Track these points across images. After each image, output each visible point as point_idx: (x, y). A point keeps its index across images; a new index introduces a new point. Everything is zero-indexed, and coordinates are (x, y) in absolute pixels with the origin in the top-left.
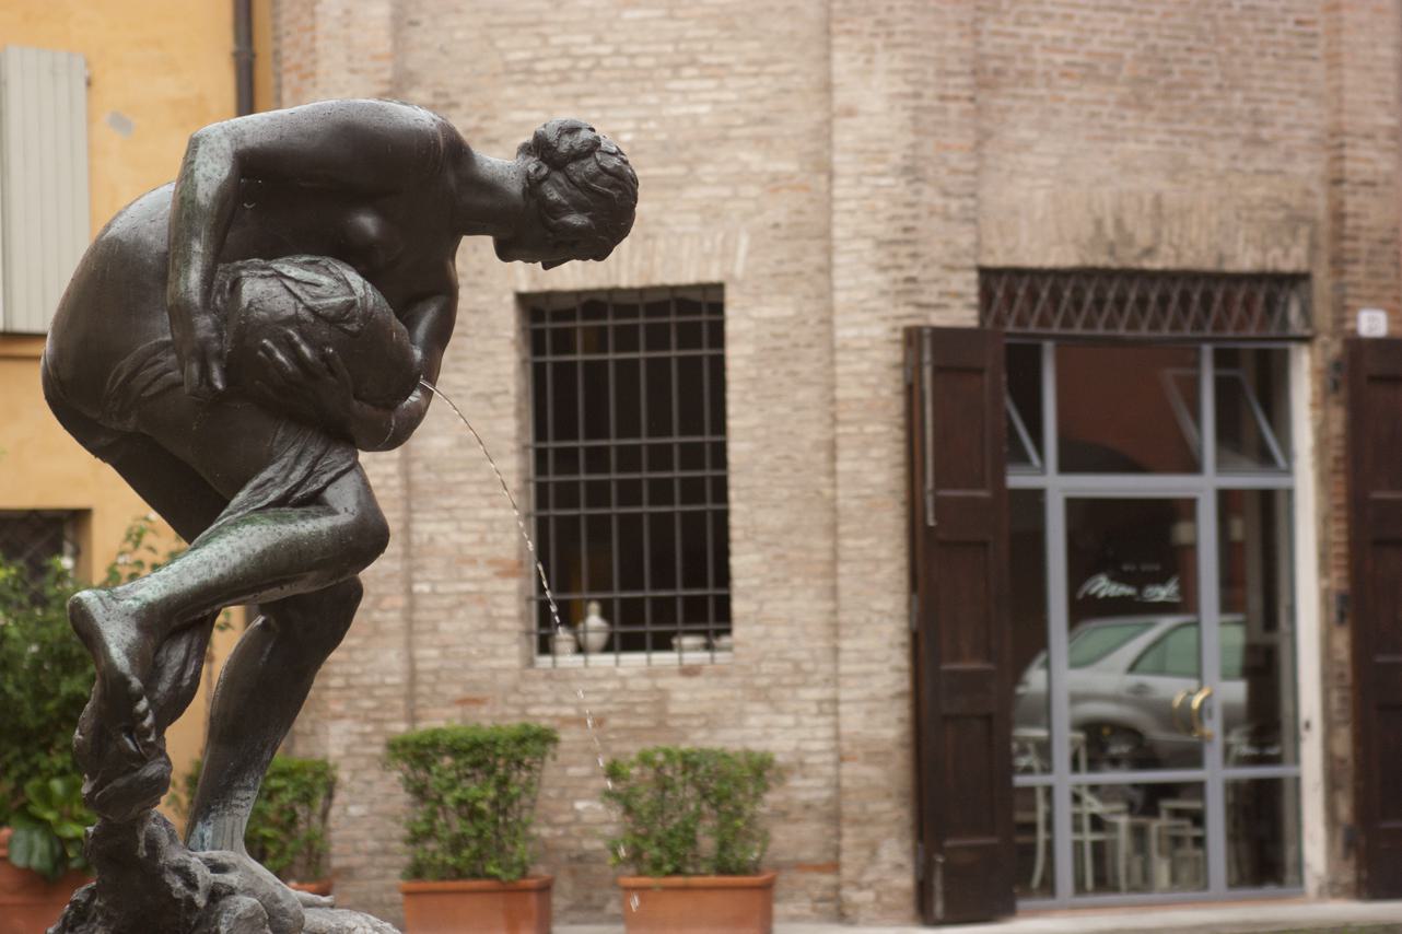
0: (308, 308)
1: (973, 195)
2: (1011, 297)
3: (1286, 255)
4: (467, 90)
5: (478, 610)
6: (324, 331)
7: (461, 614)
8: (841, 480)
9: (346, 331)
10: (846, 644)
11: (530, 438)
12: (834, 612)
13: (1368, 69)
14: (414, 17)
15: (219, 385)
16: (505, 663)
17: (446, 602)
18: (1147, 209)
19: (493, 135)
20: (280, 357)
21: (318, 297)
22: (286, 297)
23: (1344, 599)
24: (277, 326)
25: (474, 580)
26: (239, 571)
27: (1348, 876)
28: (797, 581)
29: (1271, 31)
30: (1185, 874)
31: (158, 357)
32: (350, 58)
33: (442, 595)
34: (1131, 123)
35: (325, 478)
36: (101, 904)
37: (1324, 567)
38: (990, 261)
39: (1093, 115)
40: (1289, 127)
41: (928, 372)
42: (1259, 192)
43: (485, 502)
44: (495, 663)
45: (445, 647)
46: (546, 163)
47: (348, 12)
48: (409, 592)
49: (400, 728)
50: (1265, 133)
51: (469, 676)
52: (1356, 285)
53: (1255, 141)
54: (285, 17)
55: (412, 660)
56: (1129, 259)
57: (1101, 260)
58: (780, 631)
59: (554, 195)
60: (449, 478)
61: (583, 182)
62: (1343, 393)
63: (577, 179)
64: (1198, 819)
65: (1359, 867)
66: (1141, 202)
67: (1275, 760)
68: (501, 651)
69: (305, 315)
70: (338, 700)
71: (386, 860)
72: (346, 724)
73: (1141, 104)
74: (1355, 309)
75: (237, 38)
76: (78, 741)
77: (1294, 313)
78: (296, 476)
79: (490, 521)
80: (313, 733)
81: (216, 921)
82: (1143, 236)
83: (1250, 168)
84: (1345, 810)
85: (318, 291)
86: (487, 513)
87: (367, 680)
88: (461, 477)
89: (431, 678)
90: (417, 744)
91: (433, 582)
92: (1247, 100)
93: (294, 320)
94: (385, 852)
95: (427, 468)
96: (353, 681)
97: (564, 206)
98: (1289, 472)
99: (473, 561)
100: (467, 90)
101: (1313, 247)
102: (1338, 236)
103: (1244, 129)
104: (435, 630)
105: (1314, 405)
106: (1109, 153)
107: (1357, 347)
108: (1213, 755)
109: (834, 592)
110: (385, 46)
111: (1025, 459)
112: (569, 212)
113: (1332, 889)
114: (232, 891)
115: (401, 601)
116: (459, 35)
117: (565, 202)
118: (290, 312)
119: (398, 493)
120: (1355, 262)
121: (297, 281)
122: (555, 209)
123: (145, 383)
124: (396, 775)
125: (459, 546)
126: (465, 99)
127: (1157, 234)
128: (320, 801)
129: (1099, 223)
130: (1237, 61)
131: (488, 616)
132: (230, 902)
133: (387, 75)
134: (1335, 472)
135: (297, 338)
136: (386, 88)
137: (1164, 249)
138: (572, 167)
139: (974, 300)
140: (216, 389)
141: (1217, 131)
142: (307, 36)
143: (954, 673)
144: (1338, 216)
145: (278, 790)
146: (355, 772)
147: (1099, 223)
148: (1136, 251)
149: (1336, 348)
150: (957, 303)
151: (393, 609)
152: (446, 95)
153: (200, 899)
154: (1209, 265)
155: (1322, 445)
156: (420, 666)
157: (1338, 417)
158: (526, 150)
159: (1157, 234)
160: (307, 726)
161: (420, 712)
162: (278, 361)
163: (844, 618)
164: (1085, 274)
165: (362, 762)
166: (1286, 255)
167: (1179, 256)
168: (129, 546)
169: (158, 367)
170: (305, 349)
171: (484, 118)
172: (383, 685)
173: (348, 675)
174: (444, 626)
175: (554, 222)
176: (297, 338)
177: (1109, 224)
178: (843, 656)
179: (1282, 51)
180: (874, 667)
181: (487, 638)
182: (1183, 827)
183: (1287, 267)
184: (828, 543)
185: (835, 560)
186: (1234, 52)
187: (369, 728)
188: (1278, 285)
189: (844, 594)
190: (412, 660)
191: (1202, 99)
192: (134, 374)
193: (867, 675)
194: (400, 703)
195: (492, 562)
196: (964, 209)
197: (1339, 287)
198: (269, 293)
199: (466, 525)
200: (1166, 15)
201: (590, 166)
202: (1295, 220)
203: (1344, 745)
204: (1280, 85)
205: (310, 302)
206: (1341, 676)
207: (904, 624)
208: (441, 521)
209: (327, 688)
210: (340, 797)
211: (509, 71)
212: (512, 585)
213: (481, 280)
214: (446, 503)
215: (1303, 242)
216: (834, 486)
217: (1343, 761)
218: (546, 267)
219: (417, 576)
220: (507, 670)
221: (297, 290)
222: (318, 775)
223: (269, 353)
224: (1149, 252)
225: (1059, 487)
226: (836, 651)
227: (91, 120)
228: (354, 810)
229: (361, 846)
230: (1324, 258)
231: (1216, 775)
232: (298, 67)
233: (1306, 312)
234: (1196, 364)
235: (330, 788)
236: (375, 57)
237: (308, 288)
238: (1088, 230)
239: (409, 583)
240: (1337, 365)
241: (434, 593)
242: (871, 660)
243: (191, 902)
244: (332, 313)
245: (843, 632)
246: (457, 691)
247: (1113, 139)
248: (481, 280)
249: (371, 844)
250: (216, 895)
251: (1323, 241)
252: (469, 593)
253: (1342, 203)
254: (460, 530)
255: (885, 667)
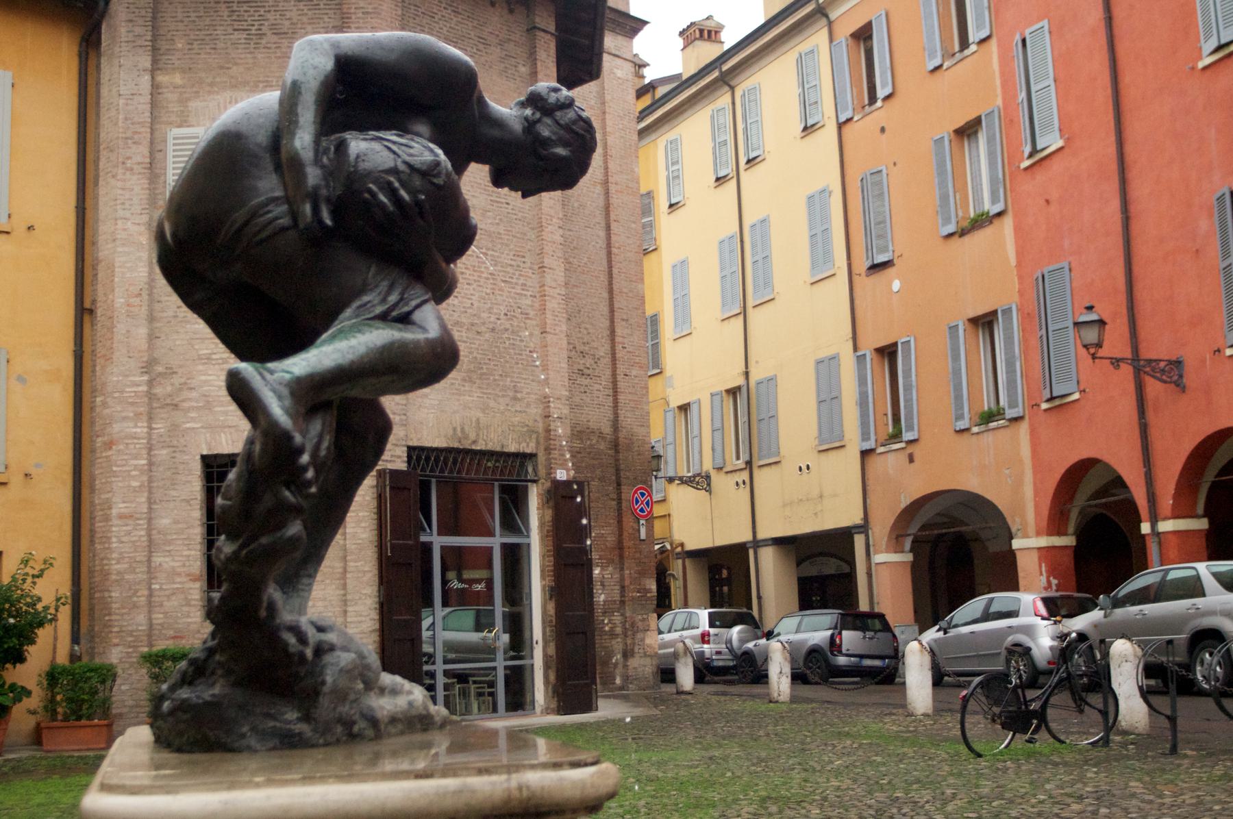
0: (405, 163)
1: (405, 415)
2: (419, 459)
3: (528, 446)
4: (181, 367)
5: (182, 596)
6: (417, 182)
7: (174, 598)
8: (348, 537)
9: (434, 184)
10: (350, 609)
11: (205, 520)
12: (345, 595)
13: (558, 372)
14: (158, 335)
15: (329, 222)
16: (194, 620)
17: (167, 593)
18: (474, 424)
19: (192, 386)
20: (382, 198)
21: (411, 155)
22: (386, 153)
23: (552, 589)
24: (384, 178)
25: (179, 583)
26: (366, 360)
27: (554, 705)
28: (328, 581)
29: (521, 355)
30: (483, 708)
31: (270, 208)
32: (128, 352)
33: (165, 590)
34: (467, 388)
35: (414, 303)
36: (222, 659)
37: (543, 577)
38: (411, 444)
39: (452, 384)
40: (528, 393)
41: (388, 489)
42: (516, 420)
43: (185, 548)
44: (189, 620)
45: (165, 613)
46: (538, 110)
47: (128, 331)
48: (150, 589)
49: (146, 649)
50: (519, 395)
51: (176, 626)
52: (555, 459)
53: (515, 399)
54: (99, 334)
55: (150, 619)
56: (466, 445)
57: (456, 445)
58: (320, 604)
59: (546, 133)
60: (169, 537)
61: (567, 124)
62: (551, 504)
63: (562, 122)
64: (492, 684)
65: (559, 701)
66: (471, 421)
67: (521, 658)
68: (192, 615)
69: (402, 167)
70: (116, 637)
71: (138, 710)
72: (120, 648)
73: (471, 381)
74: (556, 469)
75: (75, 344)
76: (222, 507)
77: (530, 470)
78: (393, 298)
79: (189, 556)
80: (104, 653)
81: (321, 673)
82: (472, 436)
83: (513, 410)
84: (552, 677)
85: (412, 151)
86: (186, 553)
87: (130, 628)
88: (174, 537)
89: (160, 627)
90: (157, 655)
91: (162, 584)
92: (512, 381)
93: (394, 171)
94: (137, 706)
95: (159, 533)
96: (124, 629)
97: (552, 140)
98: (528, 536)
99: (179, 574)
100: (181, 367)
101: (538, 443)
102: (548, 439)
103: (511, 394)
104: (161, 605)
105: (538, 509)
106: (458, 400)
107: (557, 484)
108: (500, 656)
109: (344, 586)
110: (144, 346)
111: (424, 530)
112: (556, 146)
113: (547, 711)
114: (332, 648)
115: (146, 592)
116: (177, 343)
117: (554, 138)
118: (390, 164)
119: (146, 544)
120: (555, 449)
121: (394, 143)
122: (545, 143)
123: (257, 228)
124: (144, 671)
125: (173, 568)
126: (180, 371)
127: (478, 435)
128: (109, 683)
129: (455, 429)
130: (508, 365)
131: (186, 598)
132: (328, 658)
133: (145, 359)
134: (547, 536)
135: (397, 184)
136: (144, 365)
137: (481, 441)
138: (558, 114)
139: (406, 459)
140: (326, 226)
141: (500, 394)
142: (109, 342)
143: (397, 620)
144: (548, 431)
145: (90, 678)
146: (124, 670)
147: (455, 429)
148: (470, 442)
149: (548, 484)
150: (399, 460)
151: (142, 596)
152: (171, 368)
153: (309, 653)
154: (498, 449)
155: (542, 525)
156: (155, 622)
157: (549, 514)
158: (523, 105)
159: (478, 435)
160: (101, 650)
161: (154, 643)
162: (382, 202)
163: (349, 597)
164: (449, 450)
165: (127, 666)
166: (528, 446)
167: (486, 444)
168: (22, 566)
169: (270, 215)
170: (403, 193)
171: (188, 379)
172: (138, 630)
173: (121, 626)
174: (165, 603)
175: (545, 152)
176: (397, 184)
177: (459, 429)
178: (348, 614)
179: (525, 363)
180: (364, 619)
181: (185, 609)
182: (483, 688)
183: (528, 451)
184: (342, 565)
185: (345, 571)
186: (507, 362)
187: (130, 650)
188: (524, 458)
189: (349, 587)
190: (150, 619)
191: (495, 380)
192: (247, 223)
193: (360, 622)
194: (145, 638)
195: (188, 575)
196: (401, 420)
197: (548, 460)
198: (372, 150)
199: (176, 558)
200: (479, 345)
201: (571, 115)
202: (532, 431)
203: (552, 650)
204: (524, 376)
205: (408, 159)
206: (551, 621)
207: (377, 600)
208: (164, 556)
209: (111, 632)
210: (118, 681)
211: (200, 358)
212: (197, 585)
213: (185, 449)
214: (168, 548)
215: (534, 441)
216: (345, 539)
217: (551, 657)
218: (524, 196)
219: (153, 581)
220: (195, 623)
221: (394, 148)
222: (109, 671)
223: (373, 195)
224: (474, 442)
225: (437, 541)
226: (345, 612)
227: (8, 378)
228: (123, 688)
229: (126, 703)
230: (542, 448)
231: (500, 664)
232: (104, 356)
233: (535, 470)
234: (493, 493)
235: (114, 677)
236: (139, 351)
237: (403, 148)
238: (451, 432)
239: (150, 584)
240: (549, 491)
241: (161, 589)
242: (361, 616)
243: (302, 656)
244: (424, 168)
245: (349, 603)
246: (171, 633)
247: (460, 395)
248: (185, 449)
249: (131, 703)
250: (320, 650)
251: (542, 441)
252: (177, 588)
253: (549, 425)
254: (173, 560)
255: (368, 618)
